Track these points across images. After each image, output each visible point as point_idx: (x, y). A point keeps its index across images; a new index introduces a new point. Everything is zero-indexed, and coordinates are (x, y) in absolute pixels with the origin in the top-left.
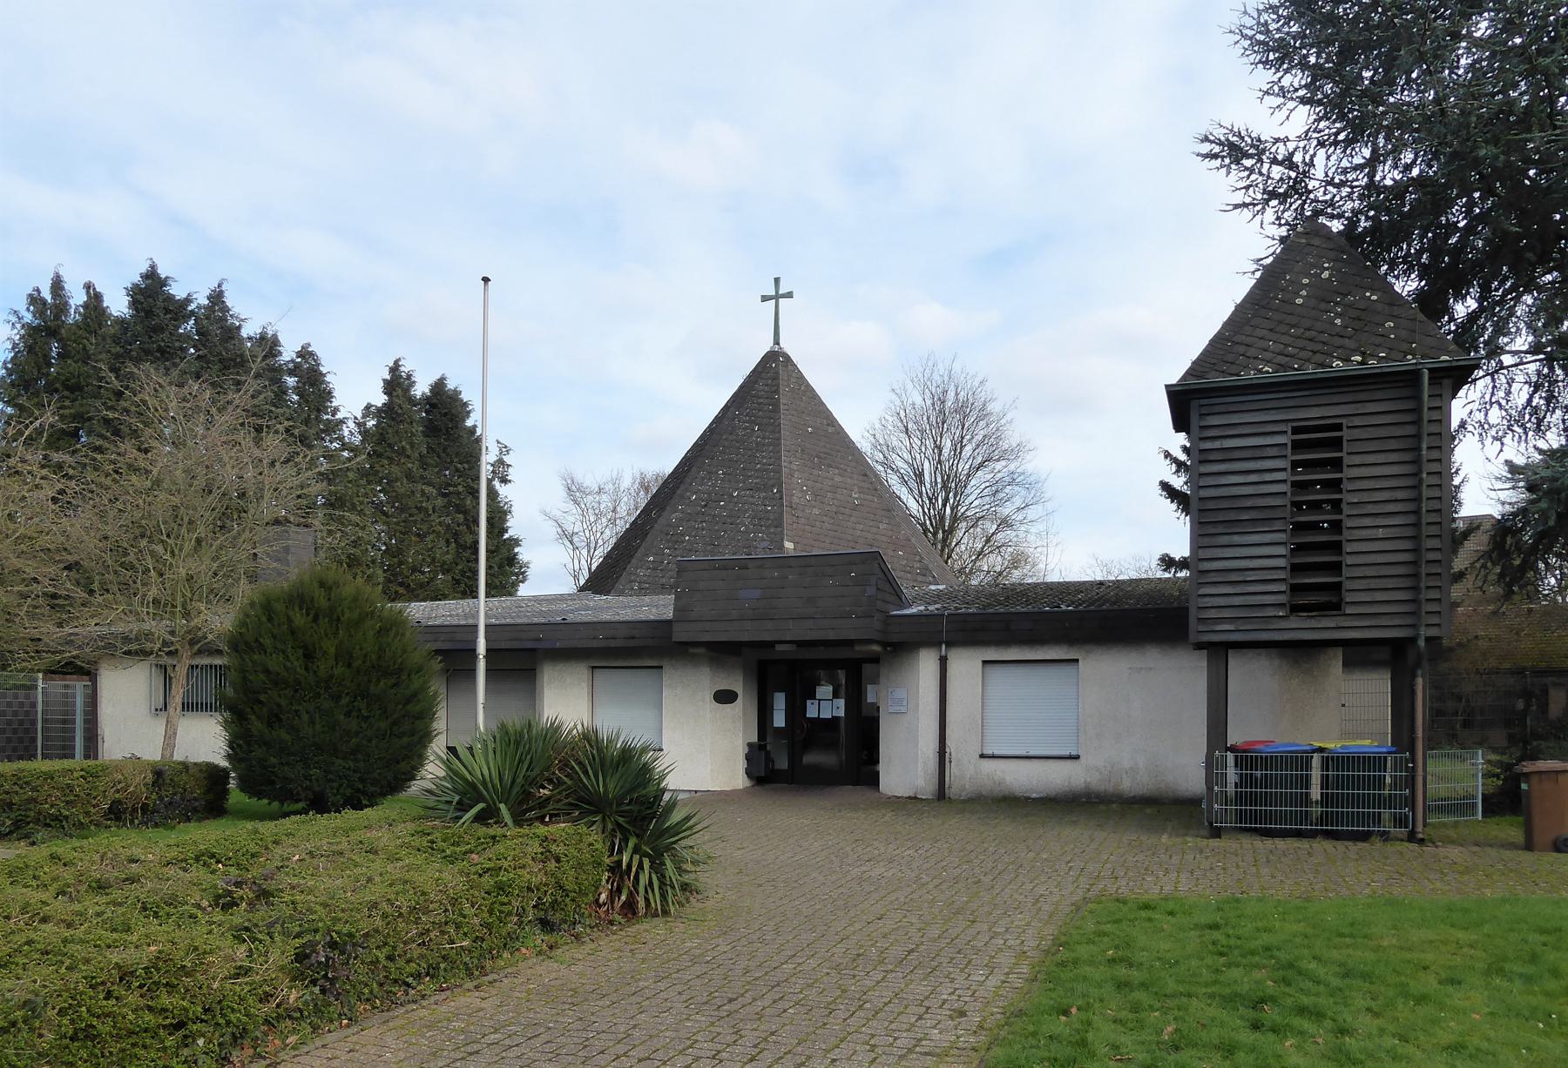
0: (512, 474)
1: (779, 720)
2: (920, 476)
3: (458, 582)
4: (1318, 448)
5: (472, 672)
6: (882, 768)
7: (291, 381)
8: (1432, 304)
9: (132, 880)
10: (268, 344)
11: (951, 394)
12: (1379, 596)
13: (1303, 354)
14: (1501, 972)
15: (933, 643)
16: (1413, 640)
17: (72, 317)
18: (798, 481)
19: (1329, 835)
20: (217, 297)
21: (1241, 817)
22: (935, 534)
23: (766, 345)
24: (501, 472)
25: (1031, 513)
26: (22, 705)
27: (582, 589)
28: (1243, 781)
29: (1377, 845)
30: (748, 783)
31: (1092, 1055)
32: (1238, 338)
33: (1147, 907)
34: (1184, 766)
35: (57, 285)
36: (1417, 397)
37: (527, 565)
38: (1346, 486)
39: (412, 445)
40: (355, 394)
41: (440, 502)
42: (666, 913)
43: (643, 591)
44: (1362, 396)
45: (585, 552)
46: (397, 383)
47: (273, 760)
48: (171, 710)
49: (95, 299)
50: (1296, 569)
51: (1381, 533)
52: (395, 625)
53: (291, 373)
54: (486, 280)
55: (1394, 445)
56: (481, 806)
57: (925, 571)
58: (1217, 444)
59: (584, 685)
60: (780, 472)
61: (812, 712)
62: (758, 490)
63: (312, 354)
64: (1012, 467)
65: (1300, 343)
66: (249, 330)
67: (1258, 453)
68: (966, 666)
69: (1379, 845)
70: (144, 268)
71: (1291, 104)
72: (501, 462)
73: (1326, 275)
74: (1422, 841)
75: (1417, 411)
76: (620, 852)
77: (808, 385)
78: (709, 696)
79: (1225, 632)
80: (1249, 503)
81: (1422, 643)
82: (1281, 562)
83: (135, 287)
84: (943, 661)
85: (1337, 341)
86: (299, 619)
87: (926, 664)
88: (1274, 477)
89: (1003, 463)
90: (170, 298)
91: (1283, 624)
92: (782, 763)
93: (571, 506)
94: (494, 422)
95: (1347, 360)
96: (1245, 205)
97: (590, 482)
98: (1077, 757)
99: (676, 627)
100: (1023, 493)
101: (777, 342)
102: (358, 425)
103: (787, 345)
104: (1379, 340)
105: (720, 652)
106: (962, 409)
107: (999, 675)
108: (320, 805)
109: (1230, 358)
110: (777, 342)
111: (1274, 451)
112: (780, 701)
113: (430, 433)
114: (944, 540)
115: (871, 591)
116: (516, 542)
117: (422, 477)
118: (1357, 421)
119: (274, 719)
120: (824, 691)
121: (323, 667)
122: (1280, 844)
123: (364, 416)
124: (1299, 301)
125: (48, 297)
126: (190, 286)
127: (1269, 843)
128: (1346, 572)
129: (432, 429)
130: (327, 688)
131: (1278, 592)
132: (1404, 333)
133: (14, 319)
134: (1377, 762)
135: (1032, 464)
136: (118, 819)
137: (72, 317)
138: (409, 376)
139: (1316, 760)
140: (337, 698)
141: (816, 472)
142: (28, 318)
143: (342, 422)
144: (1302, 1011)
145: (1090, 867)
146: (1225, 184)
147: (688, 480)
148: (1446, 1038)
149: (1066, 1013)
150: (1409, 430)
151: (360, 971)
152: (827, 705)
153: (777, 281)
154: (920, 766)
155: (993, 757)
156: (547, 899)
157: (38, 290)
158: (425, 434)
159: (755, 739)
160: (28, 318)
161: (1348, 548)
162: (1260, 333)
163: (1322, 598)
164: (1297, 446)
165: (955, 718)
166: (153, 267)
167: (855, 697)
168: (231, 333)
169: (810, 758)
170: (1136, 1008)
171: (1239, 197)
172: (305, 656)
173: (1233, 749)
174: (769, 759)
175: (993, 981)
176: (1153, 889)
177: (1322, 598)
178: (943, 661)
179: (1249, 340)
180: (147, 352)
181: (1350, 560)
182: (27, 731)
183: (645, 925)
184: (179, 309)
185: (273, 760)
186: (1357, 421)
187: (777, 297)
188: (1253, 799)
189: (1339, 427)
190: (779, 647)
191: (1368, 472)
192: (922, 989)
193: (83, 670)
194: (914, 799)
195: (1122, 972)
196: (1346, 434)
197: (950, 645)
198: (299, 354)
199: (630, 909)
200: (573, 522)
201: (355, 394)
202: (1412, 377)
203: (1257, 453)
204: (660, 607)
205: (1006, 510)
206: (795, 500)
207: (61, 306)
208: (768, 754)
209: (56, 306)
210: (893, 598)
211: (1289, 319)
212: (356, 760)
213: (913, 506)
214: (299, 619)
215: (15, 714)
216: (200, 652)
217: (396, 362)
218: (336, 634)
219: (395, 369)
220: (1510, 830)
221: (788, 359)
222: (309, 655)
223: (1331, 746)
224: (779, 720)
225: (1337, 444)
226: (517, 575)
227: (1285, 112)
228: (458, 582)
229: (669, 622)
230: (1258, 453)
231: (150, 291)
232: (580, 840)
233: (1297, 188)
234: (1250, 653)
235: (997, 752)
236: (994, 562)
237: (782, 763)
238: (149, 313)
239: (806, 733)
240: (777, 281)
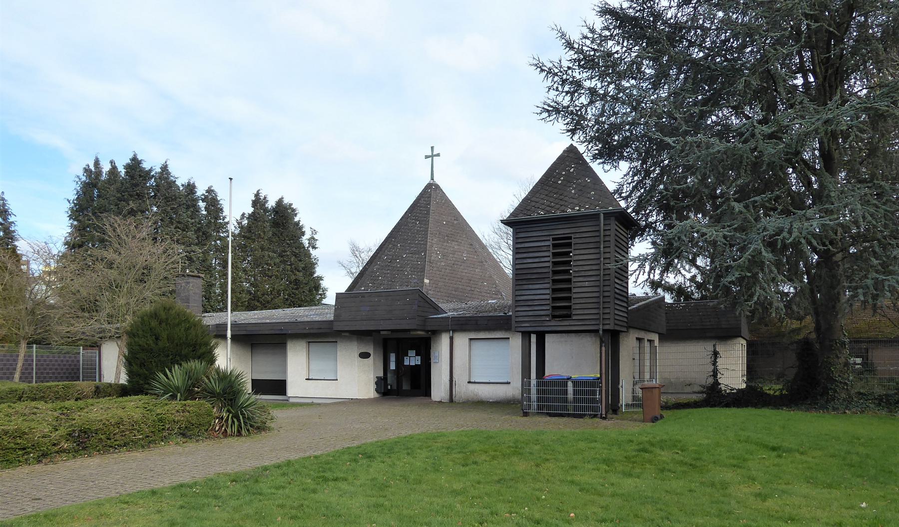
0: (318, 244)
1: (393, 366)
4: (562, 245)
7: (202, 205)
9: (35, 414)
10: (190, 188)
12: (586, 312)
13: (557, 206)
15: (447, 331)
17: (104, 177)
20: (165, 168)
23: (428, 180)
24: (313, 242)
26: (73, 361)
30: (377, 395)
35: (97, 163)
39: (264, 232)
40: (236, 210)
44: (569, 226)
46: (258, 202)
50: (554, 299)
52: (197, 325)
54: (231, 179)
55: (591, 246)
58: (523, 245)
60: (426, 245)
61: (406, 363)
62: (415, 254)
63: (213, 191)
65: (557, 201)
67: (539, 249)
68: (462, 340)
70: (131, 156)
72: (313, 238)
78: (357, 355)
82: (547, 297)
84: (451, 339)
85: (572, 200)
86: (154, 323)
87: (445, 340)
88: (545, 260)
91: (549, 324)
93: (353, 259)
94: (305, 218)
95: (573, 209)
99: (335, 323)
102: (239, 223)
103: (438, 180)
105: (360, 335)
107: (476, 345)
109: (528, 208)
111: (545, 249)
112: (393, 357)
115: (415, 307)
116: (321, 278)
120: (412, 353)
121: (160, 344)
128: (573, 301)
131: (547, 310)
134: (593, 383)
137: (104, 177)
138: (265, 198)
139: (570, 384)
142: (84, 179)
143: (228, 223)
151: (94, 441)
153: (432, 148)
154: (443, 387)
155: (475, 383)
158: (271, 227)
159: (381, 374)
160: (84, 179)
161: (574, 290)
166: (135, 155)
178: (451, 339)
179: (537, 200)
180: (131, 196)
182: (75, 373)
184: (147, 175)
187: (432, 156)
189: (570, 238)
190: (382, 333)
193: (96, 346)
194: (440, 402)
196: (573, 241)
197: (454, 331)
198: (207, 191)
201: (236, 210)
202: (595, 217)
203: (538, 249)
207: (99, 173)
210: (432, 310)
215: (70, 365)
221: (437, 187)
224: (393, 366)
230: (539, 249)
231: (135, 165)
240: (432, 148)
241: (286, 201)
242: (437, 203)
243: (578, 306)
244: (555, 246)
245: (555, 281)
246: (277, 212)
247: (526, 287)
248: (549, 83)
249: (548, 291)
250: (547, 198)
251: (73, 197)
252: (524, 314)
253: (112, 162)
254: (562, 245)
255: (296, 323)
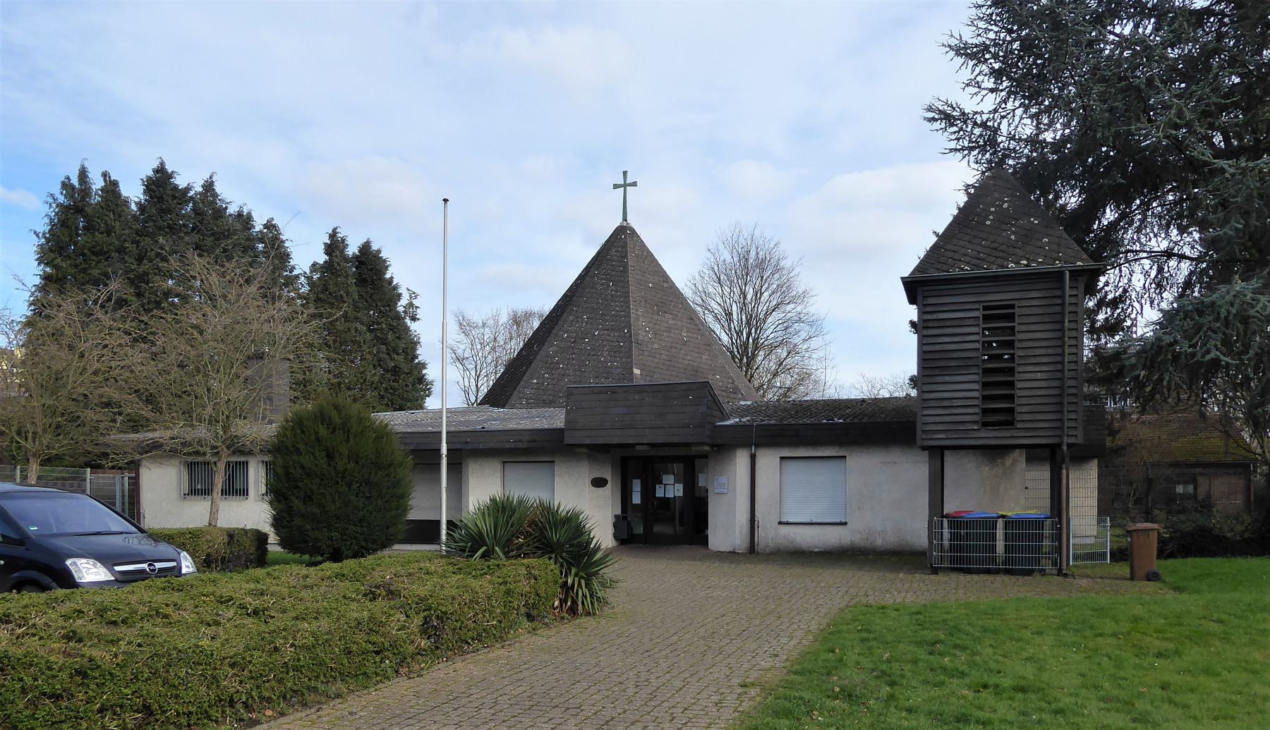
1: (637, 499)
2: (729, 314)
3: (382, 397)
5: (438, 466)
6: (710, 532)
8: (1091, 209)
11: (753, 254)
14: (1065, 628)
15: (745, 444)
16: (1059, 445)
18: (642, 322)
19: (1008, 572)
20: (209, 186)
21: (952, 560)
22: (741, 360)
23: (617, 222)
25: (814, 343)
27: (482, 403)
28: (953, 537)
29: (1038, 576)
31: (846, 665)
32: (948, 247)
33: (883, 608)
34: (914, 529)
35: (83, 174)
36: (1062, 288)
37: (431, 383)
38: (1017, 344)
40: (306, 254)
41: (368, 336)
42: (594, 614)
43: (529, 406)
44: (1025, 287)
45: (473, 373)
46: (335, 246)
47: (308, 527)
48: (215, 494)
49: (111, 188)
50: (985, 398)
51: (1039, 376)
53: (261, 241)
54: (446, 200)
56: (484, 548)
57: (736, 391)
58: (934, 316)
59: (499, 474)
62: (613, 330)
63: (274, 226)
64: (799, 309)
66: (232, 210)
68: (768, 461)
69: (1038, 577)
70: (155, 165)
71: (984, 92)
72: (411, 305)
73: (1005, 205)
74: (1066, 575)
75: (1062, 297)
76: (566, 576)
77: (649, 251)
78: (588, 483)
79: (940, 439)
80: (955, 355)
81: (1065, 448)
82: (975, 394)
83: (149, 178)
86: (323, 432)
87: (741, 460)
89: (792, 306)
90: (176, 187)
92: (639, 530)
94: (402, 272)
95: (1017, 263)
96: (956, 150)
97: (477, 319)
98: (845, 524)
100: (807, 328)
101: (625, 219)
103: (633, 221)
104: (1038, 250)
105: (596, 452)
106: (761, 264)
108: (336, 557)
109: (943, 260)
110: (625, 219)
112: (637, 486)
113: (358, 281)
114: (748, 364)
117: (356, 318)
118: (1024, 303)
119: (308, 498)
120: (669, 479)
122: (976, 577)
123: (311, 272)
124: (988, 223)
125: (76, 184)
126: (188, 178)
127: (969, 577)
129: (361, 281)
130: (343, 478)
131: (973, 414)
132: (1054, 247)
133: (51, 200)
134: (1037, 524)
135: (815, 307)
136: (209, 567)
138: (343, 240)
139: (1000, 523)
140: (349, 485)
141: (655, 317)
142: (61, 199)
143: (297, 277)
144: (956, 646)
145: (852, 590)
146: (943, 138)
147: (560, 323)
148: (1025, 655)
149: (833, 651)
150: (1057, 309)
152: (671, 489)
153: (625, 173)
155: (788, 523)
156: (531, 601)
157: (68, 178)
159: (619, 512)
160: (61, 199)
161: (1019, 385)
162: (961, 243)
163: (1002, 418)
164: (986, 318)
165: (764, 495)
166: (162, 164)
167: (689, 481)
168: (220, 213)
169: (658, 529)
170: (870, 648)
171: (953, 145)
172: (328, 456)
173: (947, 516)
174: (630, 529)
175: (793, 643)
176: (889, 600)
177: (1002, 418)
180: (160, 228)
181: (1019, 393)
183: (583, 620)
184: (181, 195)
185: (308, 527)
186: (1024, 303)
187: (625, 186)
188: (959, 549)
189: (1012, 307)
190: (637, 448)
191: (1031, 334)
192: (754, 646)
195: (865, 635)
196: (1017, 311)
197: (757, 446)
198: (266, 226)
199: (573, 611)
200: (463, 348)
201: (306, 254)
202: (1058, 276)
203: (960, 323)
204: (555, 418)
205: (796, 340)
206: (641, 338)
208: (629, 523)
209: (82, 191)
210: (718, 414)
211: (981, 235)
212: (362, 526)
213: (725, 338)
214: (323, 432)
216: (234, 453)
217: (334, 230)
218: (348, 441)
219: (333, 235)
220: (1124, 569)
222: (330, 456)
223: (1009, 514)
224: (637, 499)
225: (1011, 317)
226: (424, 391)
227: (980, 97)
228: (382, 397)
229: (561, 430)
232: (547, 567)
233: (992, 142)
234: (963, 452)
235: (791, 520)
236: (785, 380)
237: (639, 530)
238: (160, 199)
239: (656, 509)
240: (625, 173)
241: (374, 247)
242: (637, 256)
243: (1024, 409)
244: (986, 318)
245: (987, 371)
246: (361, 263)
247: (939, 379)
248: (966, 74)
249: (976, 386)
250: (968, 245)
251: (43, 227)
252: (938, 419)
253: (105, 175)
254: (999, 316)
255: (484, 432)
